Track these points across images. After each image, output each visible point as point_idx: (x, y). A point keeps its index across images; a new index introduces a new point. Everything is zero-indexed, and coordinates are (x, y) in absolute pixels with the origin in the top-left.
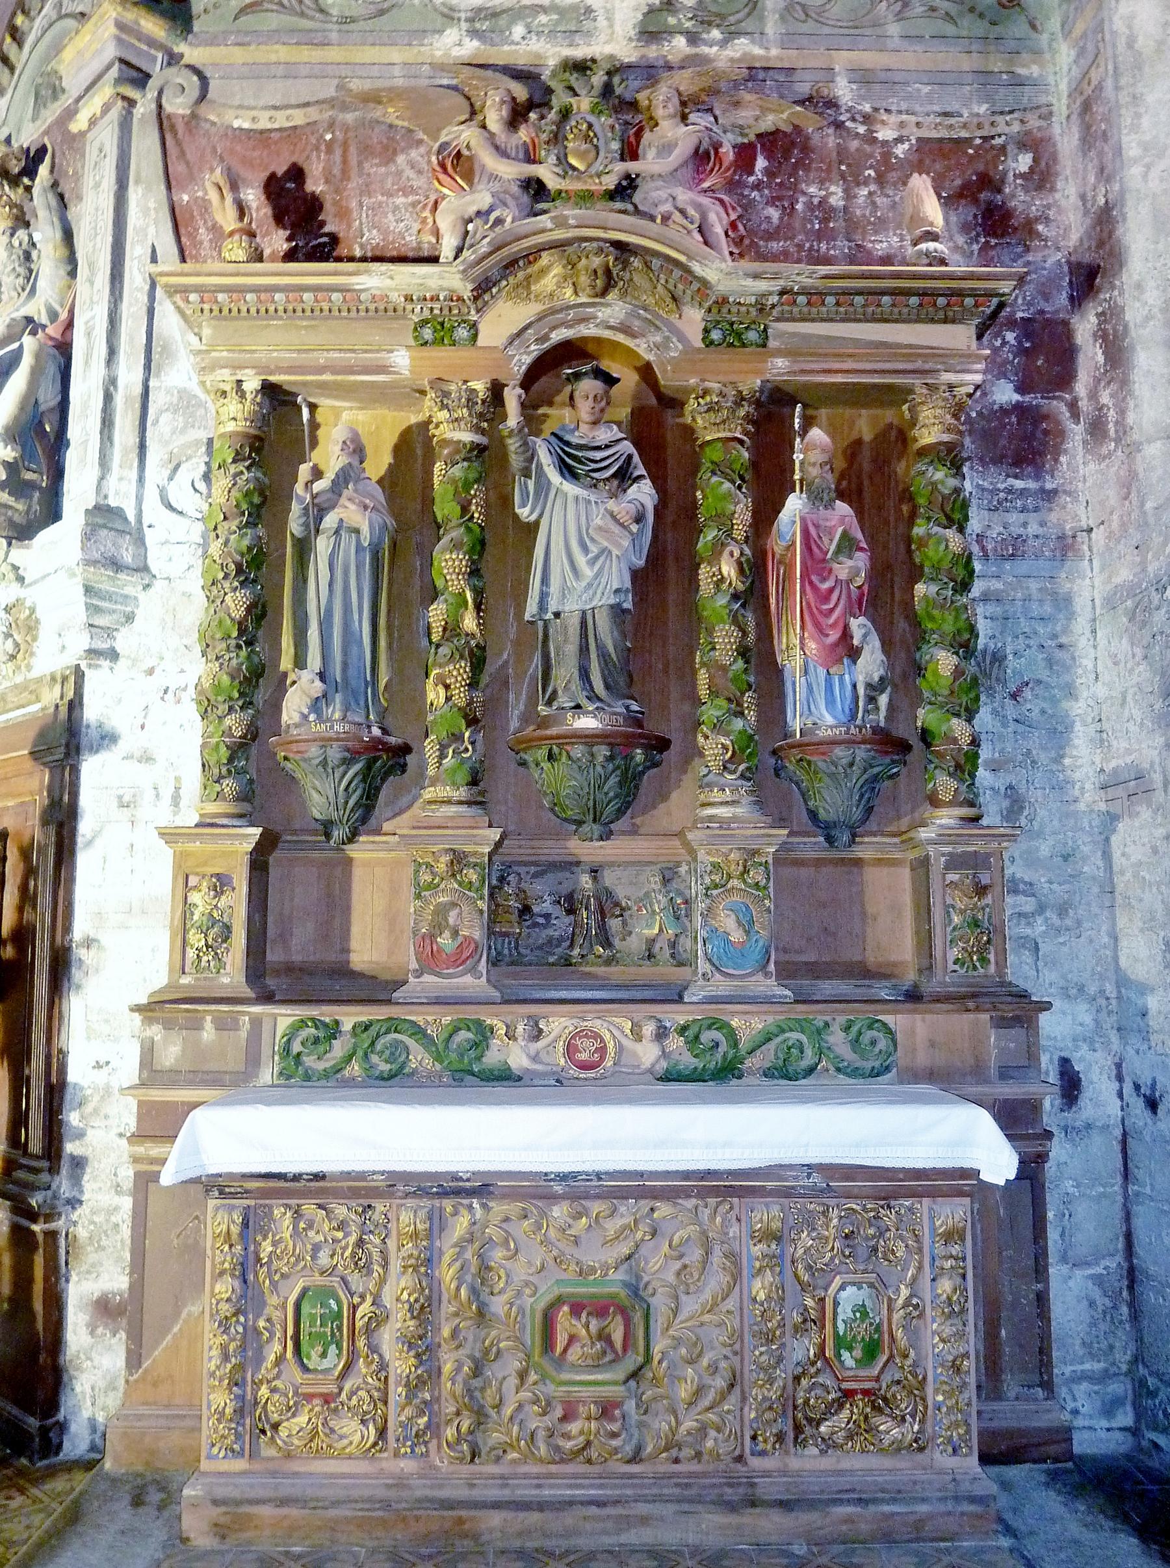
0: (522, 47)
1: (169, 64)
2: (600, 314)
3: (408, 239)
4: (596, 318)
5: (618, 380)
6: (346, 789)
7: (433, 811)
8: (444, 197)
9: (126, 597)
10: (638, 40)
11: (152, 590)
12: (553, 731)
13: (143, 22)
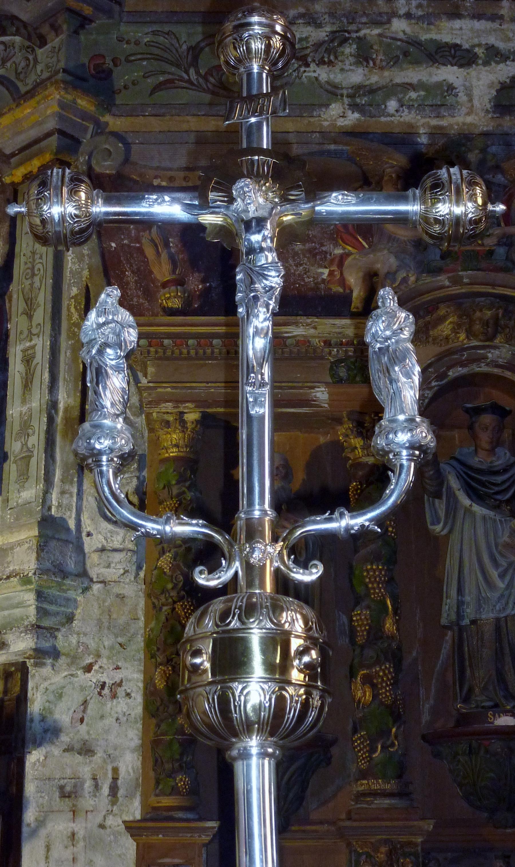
0: (396, 119)
1: (97, 134)
2: (490, 355)
3: (307, 280)
4: (487, 358)
5: (510, 412)
6: (288, 783)
7: (367, 802)
8: (349, 254)
9: (68, 600)
10: (494, 112)
11: (89, 594)
12: (477, 727)
13: (79, 101)
